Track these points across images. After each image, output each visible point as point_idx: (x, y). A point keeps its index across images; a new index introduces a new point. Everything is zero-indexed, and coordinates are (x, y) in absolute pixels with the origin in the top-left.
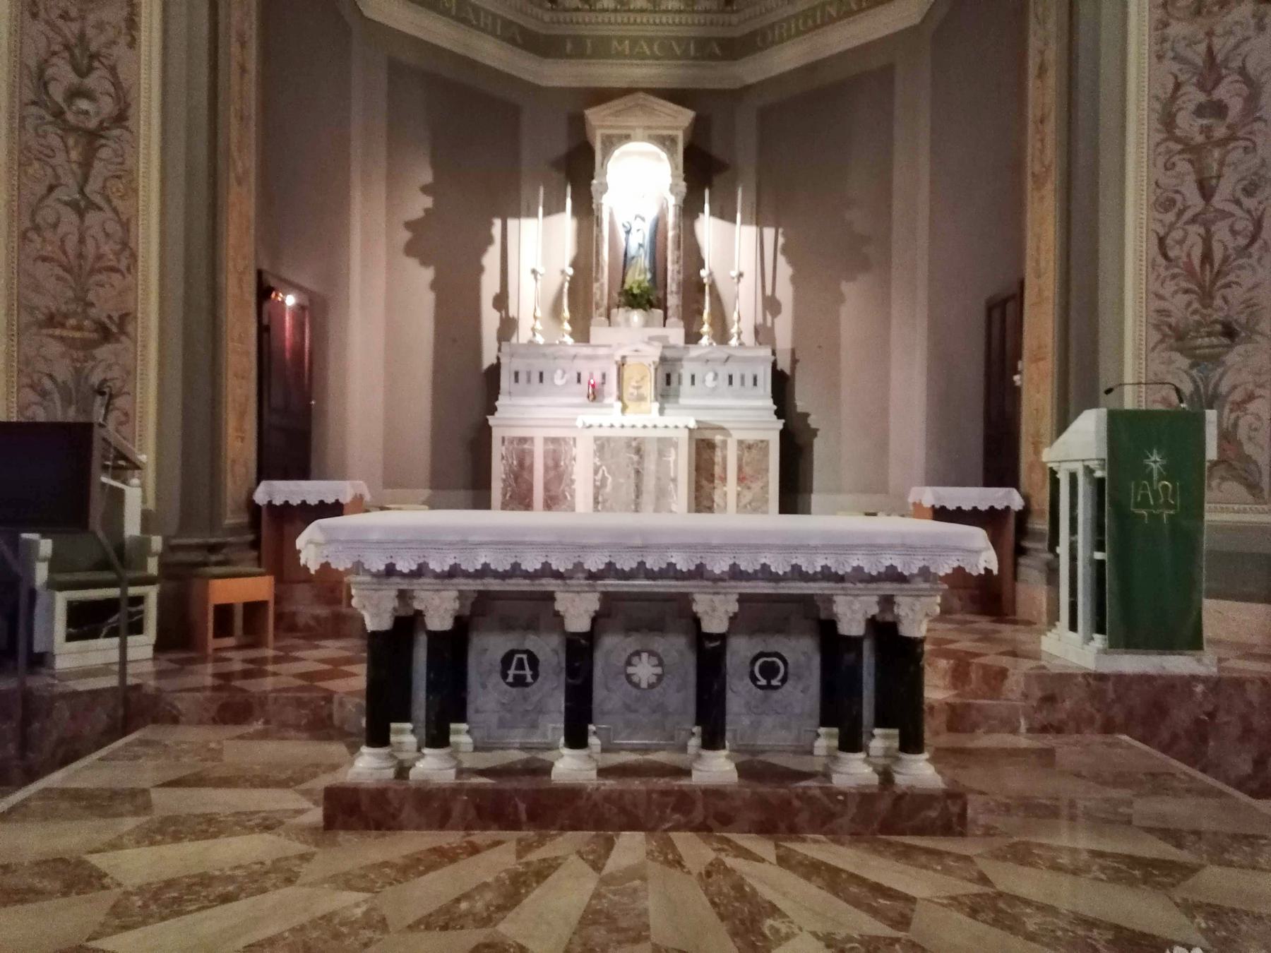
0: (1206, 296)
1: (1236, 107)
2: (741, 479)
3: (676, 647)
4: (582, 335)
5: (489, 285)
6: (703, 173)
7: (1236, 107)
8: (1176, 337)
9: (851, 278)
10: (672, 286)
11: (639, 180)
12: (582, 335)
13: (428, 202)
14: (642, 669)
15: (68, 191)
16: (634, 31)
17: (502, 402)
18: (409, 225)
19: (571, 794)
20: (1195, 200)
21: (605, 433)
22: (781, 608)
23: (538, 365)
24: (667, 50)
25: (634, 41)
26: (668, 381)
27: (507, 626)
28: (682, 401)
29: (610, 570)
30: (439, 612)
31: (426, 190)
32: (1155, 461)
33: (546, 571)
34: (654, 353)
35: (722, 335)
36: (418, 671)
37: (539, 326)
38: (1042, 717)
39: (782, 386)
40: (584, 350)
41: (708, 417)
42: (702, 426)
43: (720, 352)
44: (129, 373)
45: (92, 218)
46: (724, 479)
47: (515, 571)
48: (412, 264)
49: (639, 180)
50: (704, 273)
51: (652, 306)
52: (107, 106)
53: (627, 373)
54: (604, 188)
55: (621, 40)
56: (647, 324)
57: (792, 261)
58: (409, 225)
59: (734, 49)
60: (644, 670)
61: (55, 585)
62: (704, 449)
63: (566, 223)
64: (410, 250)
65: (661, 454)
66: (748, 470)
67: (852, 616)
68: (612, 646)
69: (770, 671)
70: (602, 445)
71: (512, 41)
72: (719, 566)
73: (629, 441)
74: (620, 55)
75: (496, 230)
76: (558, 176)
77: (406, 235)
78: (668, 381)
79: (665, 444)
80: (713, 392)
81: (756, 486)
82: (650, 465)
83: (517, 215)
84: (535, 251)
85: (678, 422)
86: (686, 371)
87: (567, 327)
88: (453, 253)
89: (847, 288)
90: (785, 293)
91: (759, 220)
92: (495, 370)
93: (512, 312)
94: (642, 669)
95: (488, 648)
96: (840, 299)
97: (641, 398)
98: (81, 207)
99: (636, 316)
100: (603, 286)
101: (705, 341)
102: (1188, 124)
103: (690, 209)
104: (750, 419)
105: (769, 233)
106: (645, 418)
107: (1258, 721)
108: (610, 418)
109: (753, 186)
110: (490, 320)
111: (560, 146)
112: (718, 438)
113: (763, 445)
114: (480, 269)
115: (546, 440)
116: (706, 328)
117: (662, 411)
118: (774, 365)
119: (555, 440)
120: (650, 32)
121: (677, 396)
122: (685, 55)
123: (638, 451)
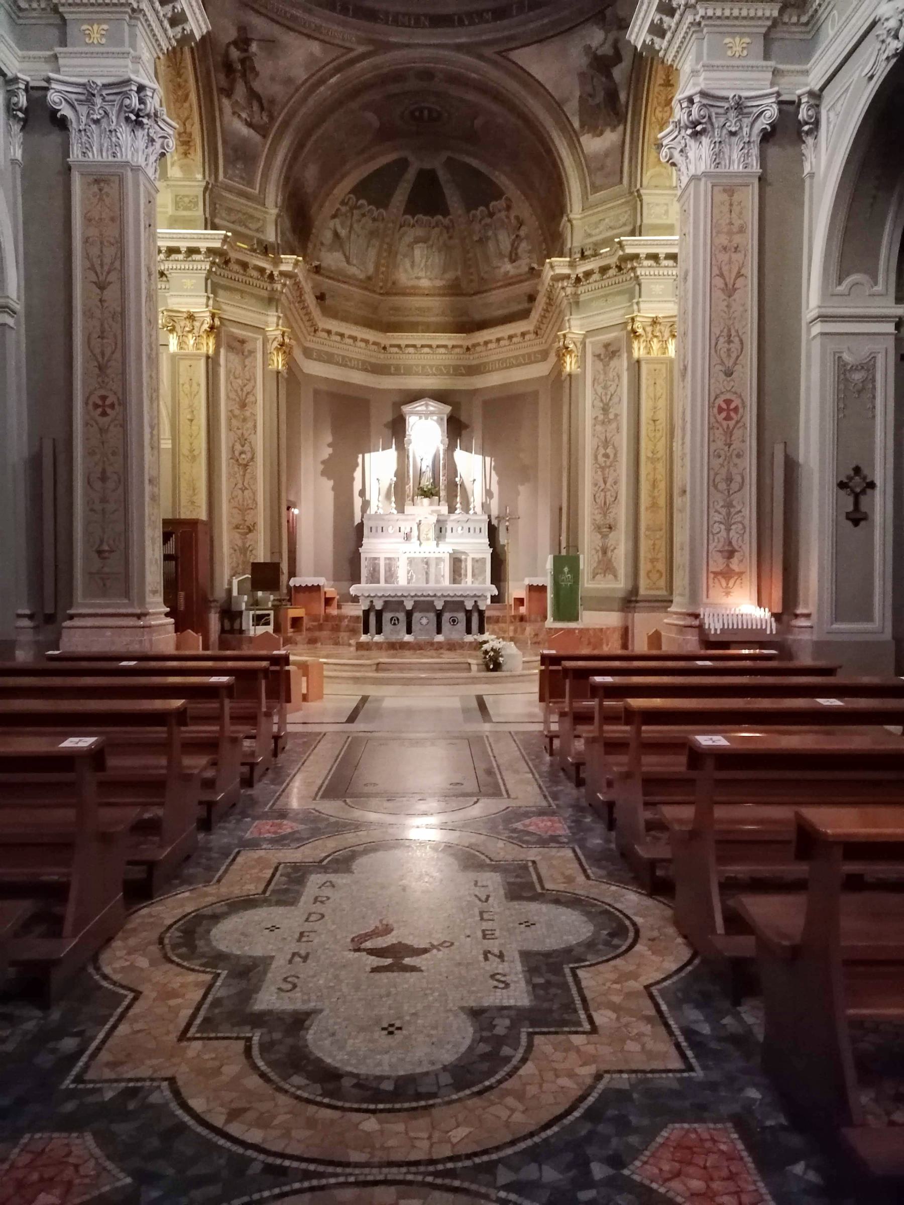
0: (605, 515)
1: (612, 456)
2: (473, 576)
3: (432, 616)
4: (401, 510)
5: (357, 486)
6: (456, 429)
7: (612, 456)
8: (598, 528)
9: (522, 484)
10: (442, 487)
11: (426, 431)
12: (401, 510)
13: (330, 450)
14: (423, 620)
15: (240, 486)
16: (424, 362)
17: (365, 541)
18: (323, 462)
19: (408, 643)
20: (603, 486)
21: (412, 555)
22: (455, 605)
23: (381, 524)
24: (439, 371)
25: (424, 367)
26: (440, 530)
27: (392, 611)
28: (447, 540)
29: (416, 595)
30: (379, 605)
31: (329, 445)
32: (566, 569)
33: (402, 596)
34: (434, 519)
35: (466, 508)
36: (372, 619)
37: (380, 505)
38: (535, 640)
39: (493, 532)
40: (401, 516)
41: (457, 548)
42: (455, 551)
43: (465, 517)
44: (256, 542)
45: (246, 492)
46: (466, 575)
47: (396, 596)
48: (324, 479)
49: (426, 431)
50: (457, 479)
51: (433, 495)
52: (249, 455)
53: (422, 528)
54: (410, 442)
55: (417, 366)
56: (431, 504)
57: (497, 474)
58: (323, 462)
59: (472, 371)
60: (424, 621)
61: (247, 609)
62: (456, 562)
63: (391, 454)
64: (324, 473)
65: (437, 564)
66: (476, 571)
67: (469, 605)
68: (416, 616)
69: (454, 621)
70: (411, 561)
71: (366, 370)
72: (439, 594)
73: (423, 559)
74: (417, 374)
75: (360, 460)
76: (388, 432)
77: (321, 467)
78: (440, 530)
79: (439, 560)
80: (462, 536)
81: (480, 579)
82: (432, 570)
83: (370, 452)
84: (378, 467)
85: (445, 549)
86: (449, 526)
87: (393, 505)
88: (341, 472)
89: (521, 488)
90: (495, 489)
91: (484, 454)
92: (361, 526)
93: (367, 498)
94: (423, 620)
95: (387, 616)
96: (518, 493)
97: (428, 539)
98: (243, 490)
99: (426, 501)
100: (410, 487)
101: (458, 511)
102: (601, 459)
103: (451, 448)
104: (477, 547)
105: (488, 459)
106: (430, 549)
107: (592, 640)
108: (413, 549)
109: (480, 441)
110: (358, 502)
111: (389, 417)
112: (463, 557)
113: (483, 560)
114: (353, 479)
115: (386, 559)
116: (458, 505)
117: (437, 545)
118: (490, 523)
119: (389, 559)
120: (432, 363)
121: (445, 537)
122: (448, 374)
123: (427, 563)
